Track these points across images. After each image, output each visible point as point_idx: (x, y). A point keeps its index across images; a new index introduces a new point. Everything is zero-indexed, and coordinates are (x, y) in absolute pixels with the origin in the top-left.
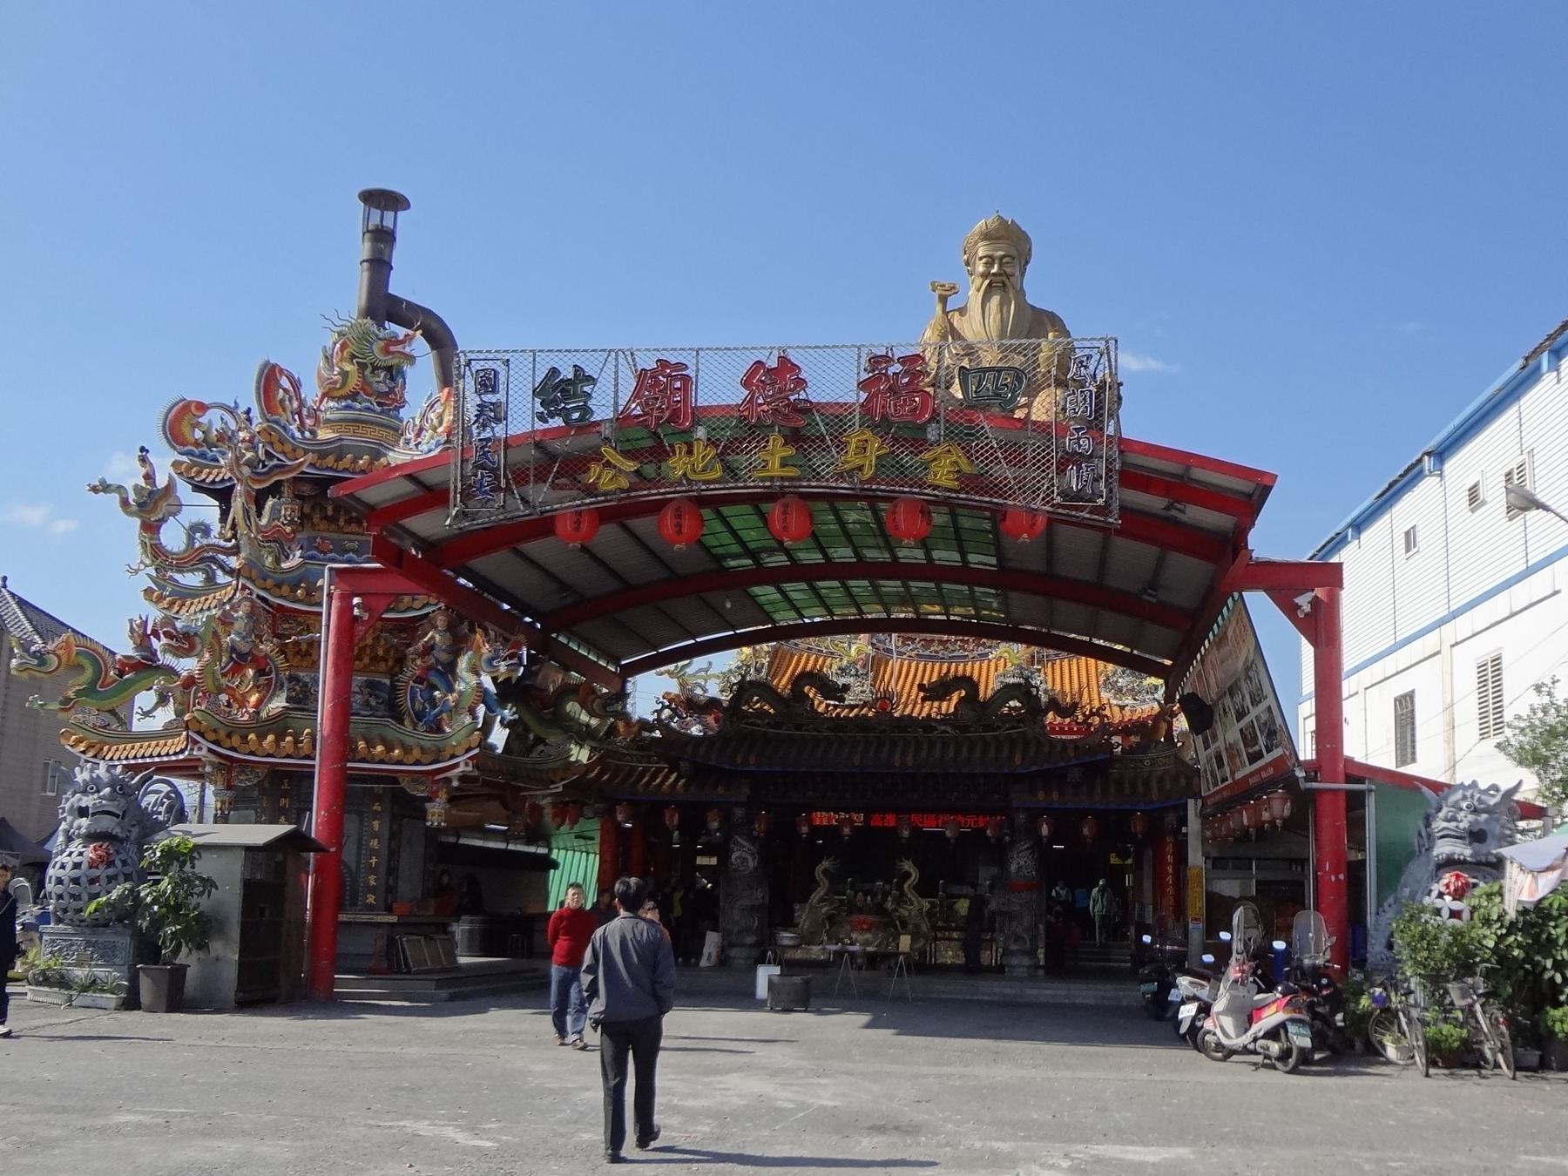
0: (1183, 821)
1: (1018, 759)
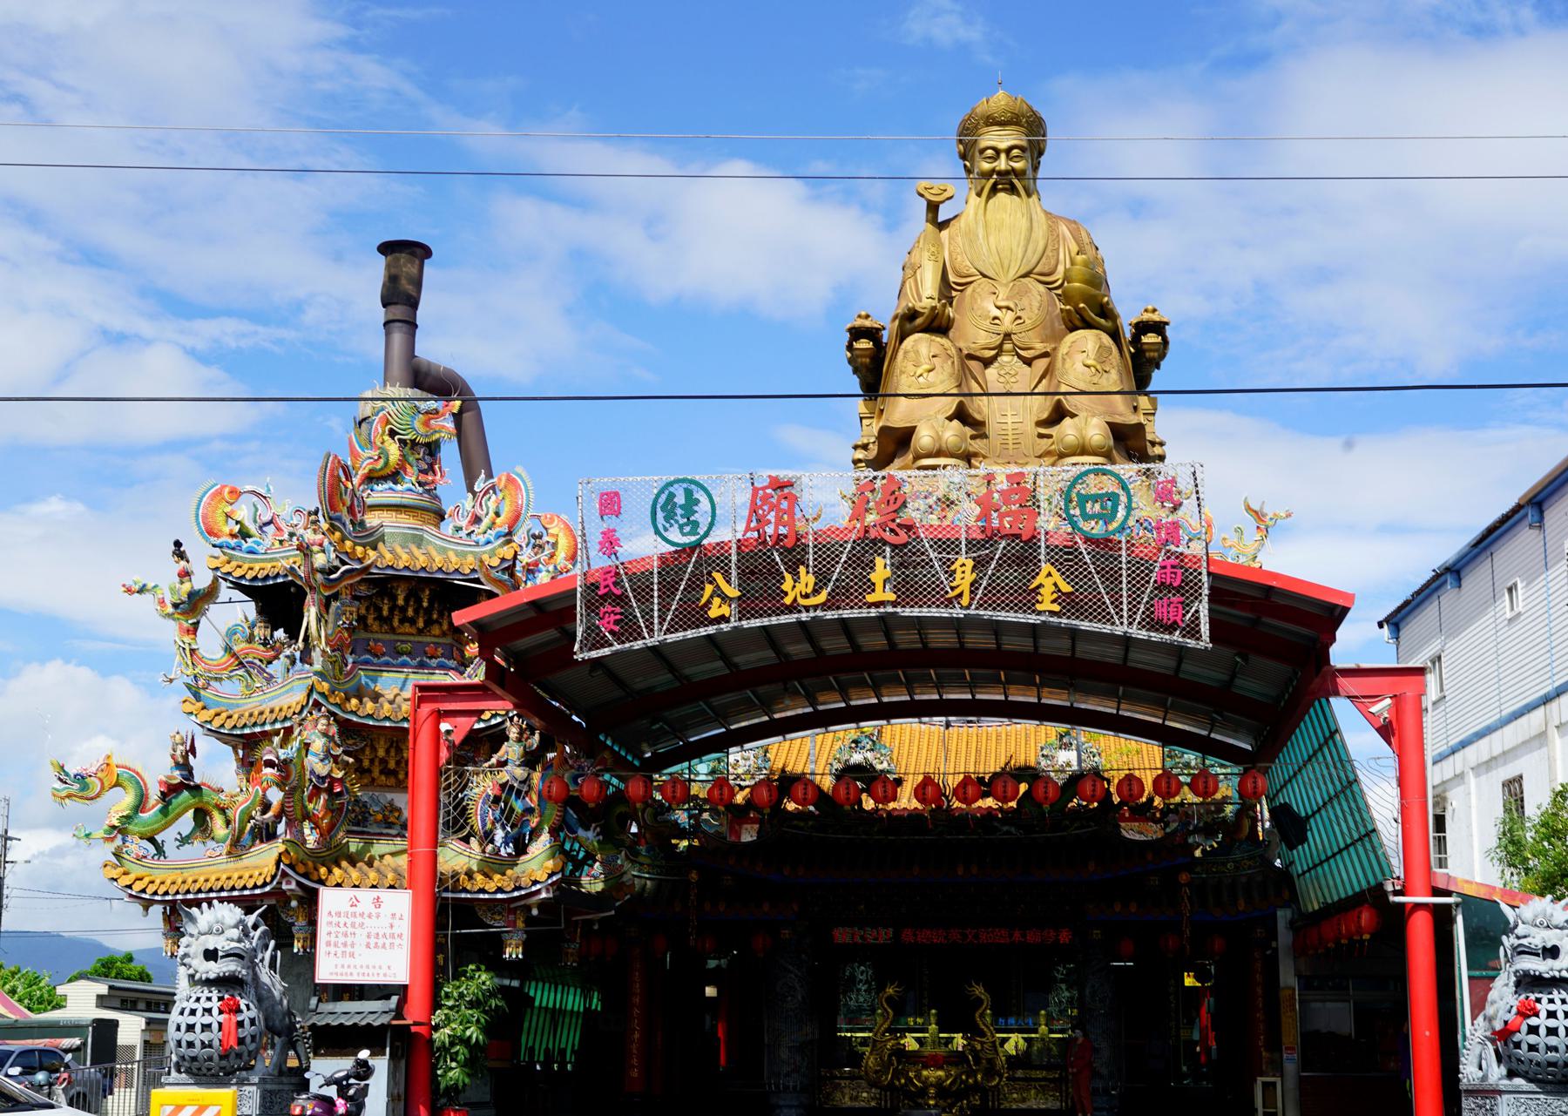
0: (1273, 935)
1: (1242, 905)
